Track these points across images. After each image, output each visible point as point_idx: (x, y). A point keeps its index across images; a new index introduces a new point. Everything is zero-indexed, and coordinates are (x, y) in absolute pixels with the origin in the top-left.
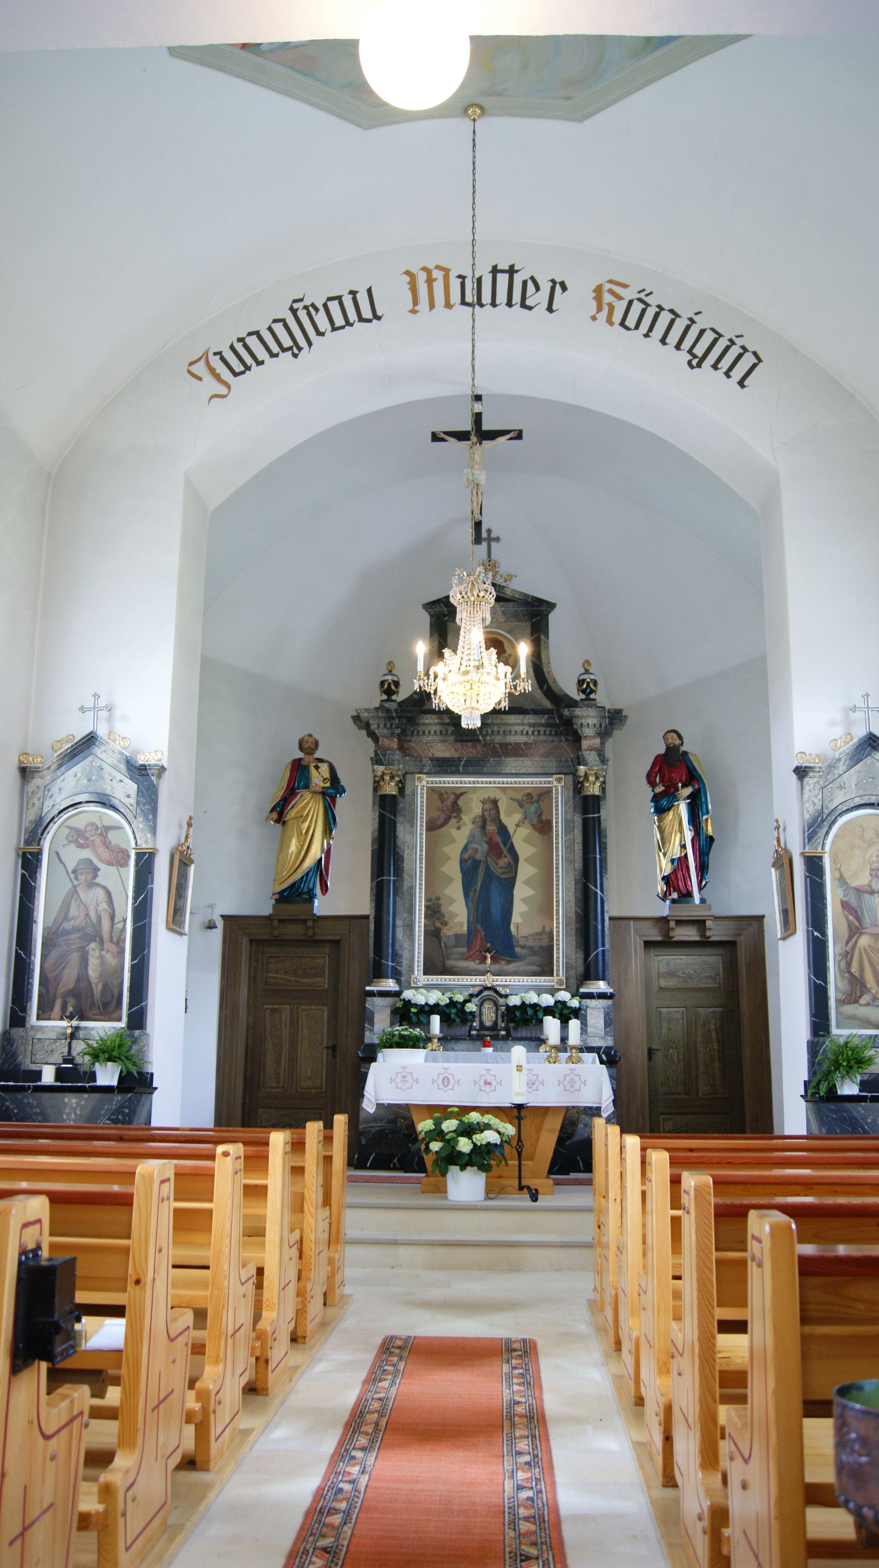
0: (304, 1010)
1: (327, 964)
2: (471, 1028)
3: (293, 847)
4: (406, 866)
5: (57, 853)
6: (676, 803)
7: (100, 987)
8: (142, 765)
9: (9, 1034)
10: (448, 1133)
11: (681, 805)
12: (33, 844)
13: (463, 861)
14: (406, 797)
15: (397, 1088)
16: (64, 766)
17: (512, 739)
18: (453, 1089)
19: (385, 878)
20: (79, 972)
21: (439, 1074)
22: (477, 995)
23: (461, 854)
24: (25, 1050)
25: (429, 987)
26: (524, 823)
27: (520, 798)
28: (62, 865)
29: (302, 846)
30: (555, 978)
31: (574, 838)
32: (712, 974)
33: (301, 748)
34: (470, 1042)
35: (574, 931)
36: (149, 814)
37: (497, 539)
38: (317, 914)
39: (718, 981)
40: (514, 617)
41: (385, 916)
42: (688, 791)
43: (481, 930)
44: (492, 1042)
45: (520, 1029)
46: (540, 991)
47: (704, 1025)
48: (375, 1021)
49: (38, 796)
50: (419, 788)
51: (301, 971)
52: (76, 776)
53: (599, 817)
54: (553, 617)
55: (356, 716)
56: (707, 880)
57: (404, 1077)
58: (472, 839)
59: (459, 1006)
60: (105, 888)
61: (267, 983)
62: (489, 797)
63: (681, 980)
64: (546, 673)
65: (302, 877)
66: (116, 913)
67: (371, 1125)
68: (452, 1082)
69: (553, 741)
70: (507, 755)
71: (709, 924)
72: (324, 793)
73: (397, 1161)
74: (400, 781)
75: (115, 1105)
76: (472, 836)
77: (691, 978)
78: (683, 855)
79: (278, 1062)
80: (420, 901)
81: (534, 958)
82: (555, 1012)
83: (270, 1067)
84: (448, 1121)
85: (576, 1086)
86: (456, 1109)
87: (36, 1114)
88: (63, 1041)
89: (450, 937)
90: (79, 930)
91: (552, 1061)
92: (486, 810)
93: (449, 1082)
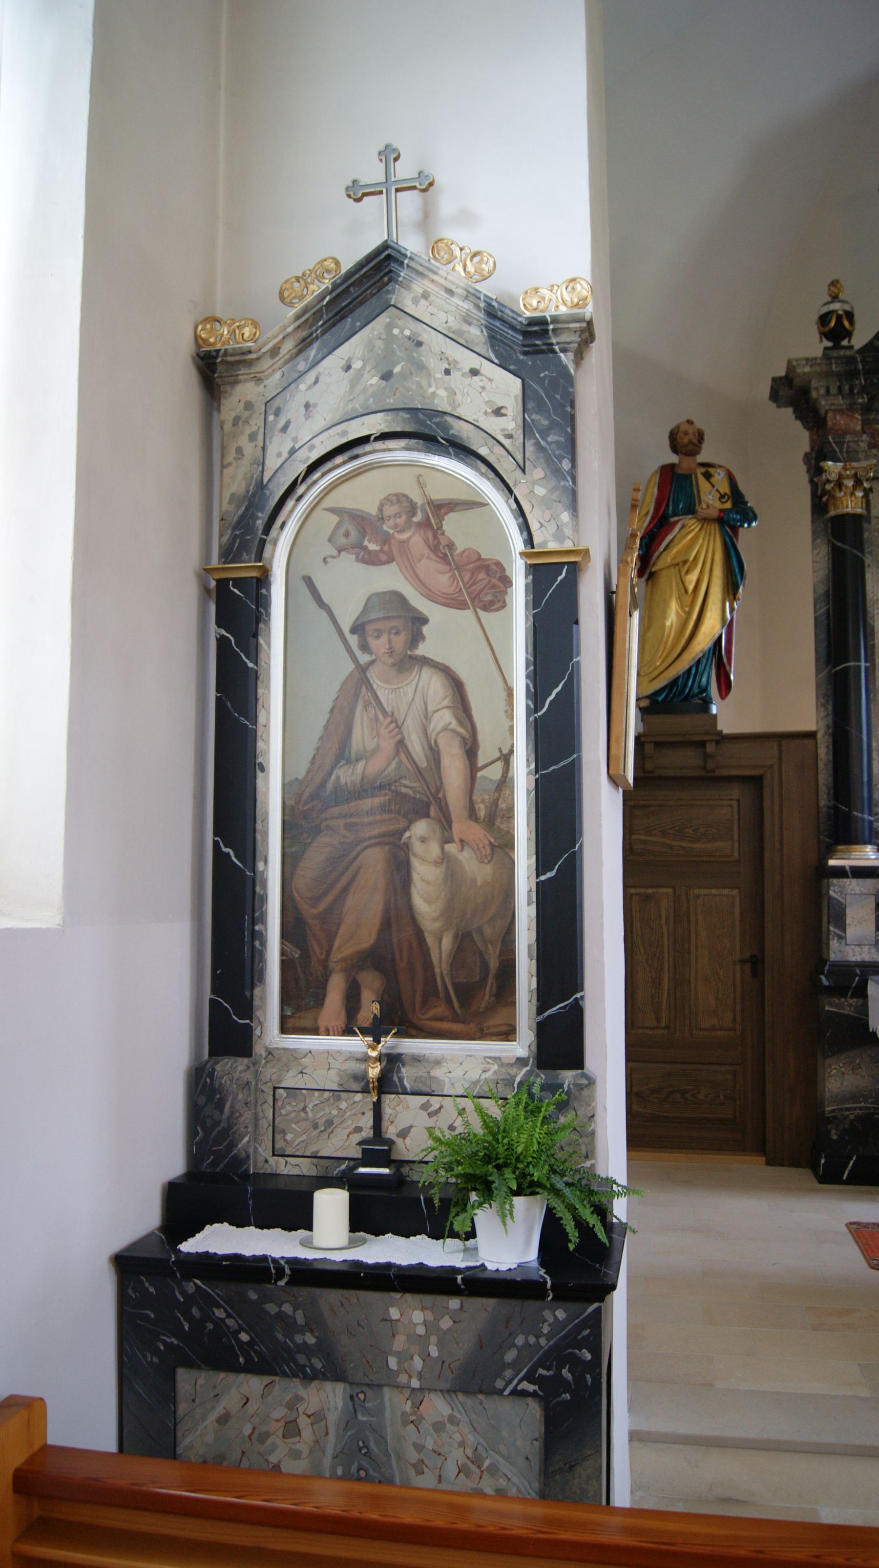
3: (672, 616)
5: (308, 581)
7: (447, 943)
8: (533, 322)
9: (211, 1075)
12: (245, 556)
16: (316, 345)
19: (852, 664)
20: (387, 903)
24: (256, 1119)
28: (323, 614)
29: (689, 614)
33: (675, 448)
36: (560, 458)
38: (725, 732)
41: (853, 731)
48: (848, 921)
49: (248, 430)
51: (690, 831)
52: (348, 368)
60: (446, 671)
65: (690, 669)
66: (480, 738)
75: (549, 1337)
87: (304, 1348)
88: (359, 1097)
90: (381, 787)
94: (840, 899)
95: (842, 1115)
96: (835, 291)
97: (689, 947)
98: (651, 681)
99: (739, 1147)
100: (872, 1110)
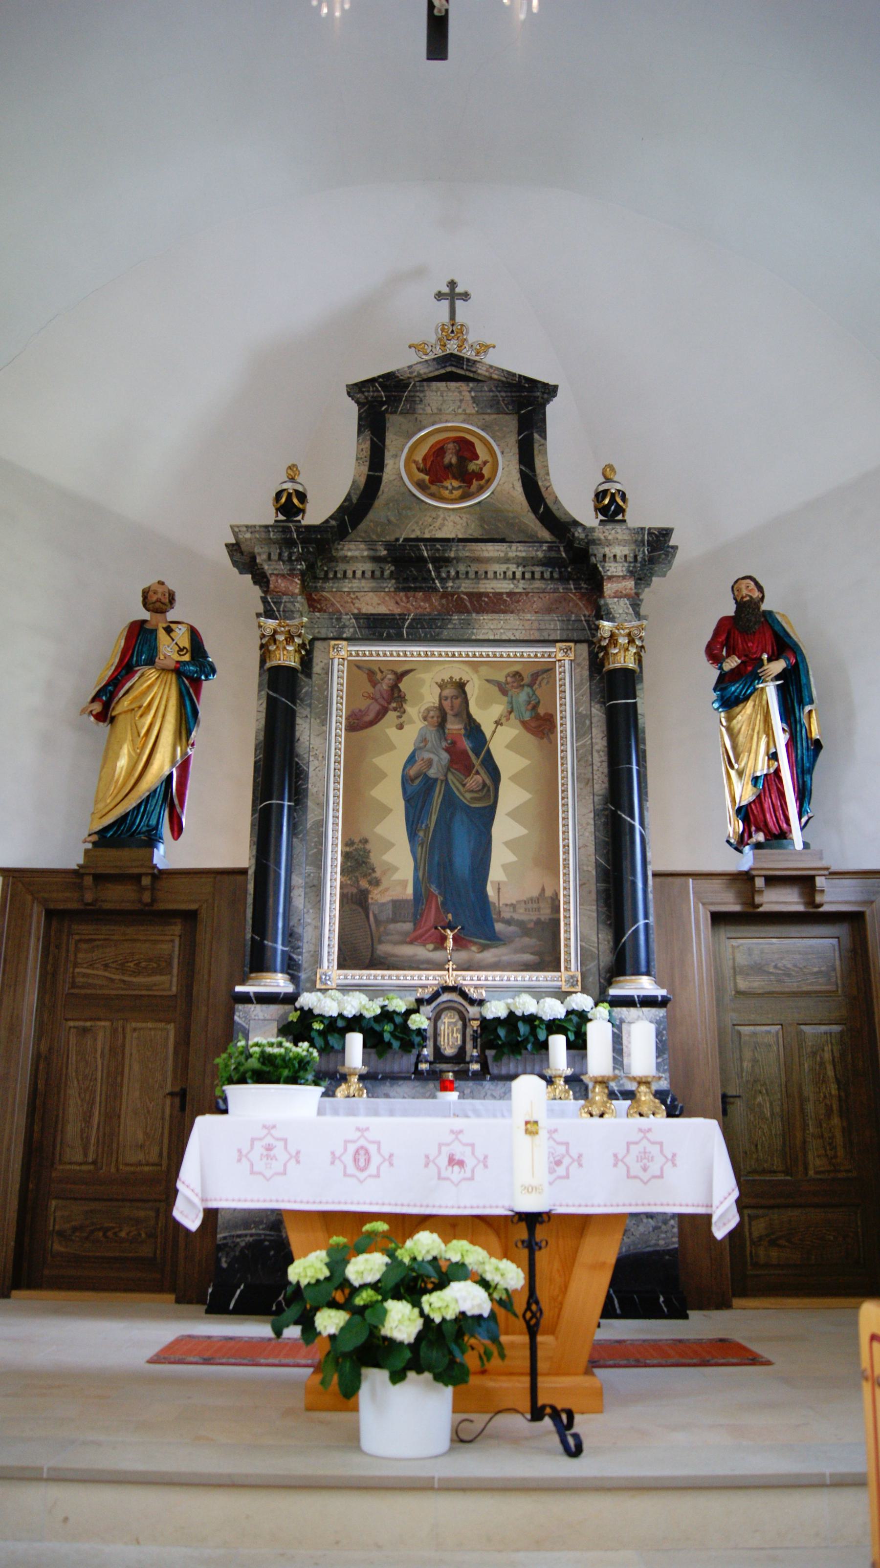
0: (135, 1030)
1: (176, 953)
2: (419, 1059)
4: (313, 786)
6: (761, 686)
10: (364, 1286)
11: (767, 688)
13: (406, 781)
14: (314, 677)
15: (252, 1172)
17: (489, 586)
18: (378, 1176)
19: (274, 802)
21: (346, 1142)
22: (430, 1001)
23: (404, 770)
25: (345, 989)
26: (508, 719)
27: (502, 679)
29: (140, 755)
30: (564, 974)
31: (592, 743)
32: (823, 969)
33: (145, 604)
34: (417, 1083)
35: (594, 896)
37: (465, 296)
39: (833, 980)
40: (491, 406)
41: (272, 866)
42: (778, 666)
43: (436, 893)
44: (456, 1084)
45: (505, 1060)
46: (538, 994)
47: (814, 1054)
50: (336, 662)
51: (132, 965)
53: (635, 704)
54: (552, 409)
55: (233, 545)
56: (810, 815)
57: (269, 1148)
58: (422, 742)
59: (398, 1020)
61: (73, 985)
62: (451, 678)
63: (772, 978)
64: (543, 490)
67: (239, 1232)
68: (376, 1160)
69: (555, 591)
70: (481, 610)
71: (820, 882)
72: (178, 671)
73: (284, 1298)
74: (303, 646)
76: (423, 740)
77: (789, 975)
78: (772, 770)
79: (87, 1118)
80: (335, 845)
81: (526, 940)
82: (568, 1030)
83: (72, 1129)
84: (362, 1258)
85: (654, 1169)
86: (382, 1226)
89: (383, 904)
91: (596, 1111)
92: (446, 698)
93: (368, 1161)
94: (244, 1024)
95: (233, 1242)
96: (292, 473)
97: (122, 1080)
98: (101, 818)
99: (157, 1287)
100: (263, 1237)
